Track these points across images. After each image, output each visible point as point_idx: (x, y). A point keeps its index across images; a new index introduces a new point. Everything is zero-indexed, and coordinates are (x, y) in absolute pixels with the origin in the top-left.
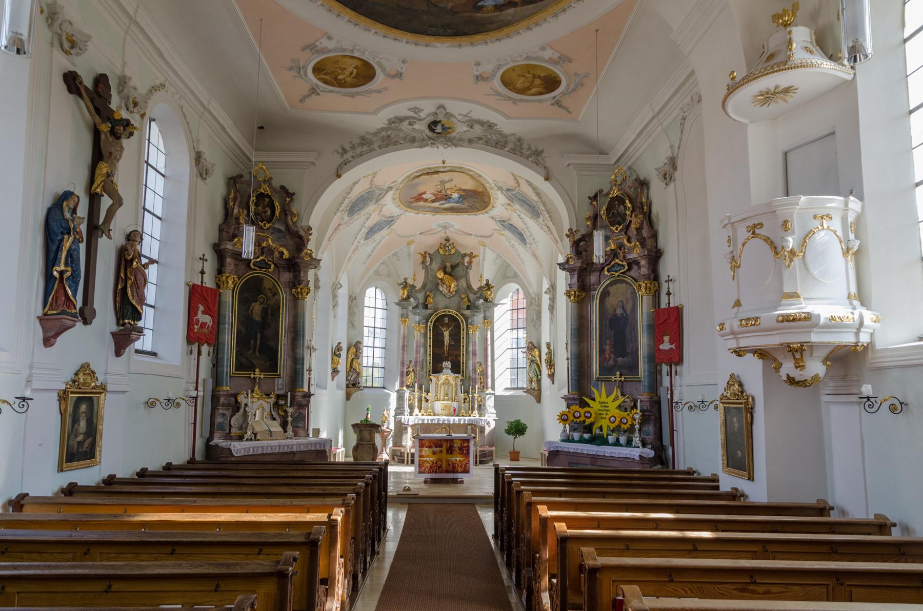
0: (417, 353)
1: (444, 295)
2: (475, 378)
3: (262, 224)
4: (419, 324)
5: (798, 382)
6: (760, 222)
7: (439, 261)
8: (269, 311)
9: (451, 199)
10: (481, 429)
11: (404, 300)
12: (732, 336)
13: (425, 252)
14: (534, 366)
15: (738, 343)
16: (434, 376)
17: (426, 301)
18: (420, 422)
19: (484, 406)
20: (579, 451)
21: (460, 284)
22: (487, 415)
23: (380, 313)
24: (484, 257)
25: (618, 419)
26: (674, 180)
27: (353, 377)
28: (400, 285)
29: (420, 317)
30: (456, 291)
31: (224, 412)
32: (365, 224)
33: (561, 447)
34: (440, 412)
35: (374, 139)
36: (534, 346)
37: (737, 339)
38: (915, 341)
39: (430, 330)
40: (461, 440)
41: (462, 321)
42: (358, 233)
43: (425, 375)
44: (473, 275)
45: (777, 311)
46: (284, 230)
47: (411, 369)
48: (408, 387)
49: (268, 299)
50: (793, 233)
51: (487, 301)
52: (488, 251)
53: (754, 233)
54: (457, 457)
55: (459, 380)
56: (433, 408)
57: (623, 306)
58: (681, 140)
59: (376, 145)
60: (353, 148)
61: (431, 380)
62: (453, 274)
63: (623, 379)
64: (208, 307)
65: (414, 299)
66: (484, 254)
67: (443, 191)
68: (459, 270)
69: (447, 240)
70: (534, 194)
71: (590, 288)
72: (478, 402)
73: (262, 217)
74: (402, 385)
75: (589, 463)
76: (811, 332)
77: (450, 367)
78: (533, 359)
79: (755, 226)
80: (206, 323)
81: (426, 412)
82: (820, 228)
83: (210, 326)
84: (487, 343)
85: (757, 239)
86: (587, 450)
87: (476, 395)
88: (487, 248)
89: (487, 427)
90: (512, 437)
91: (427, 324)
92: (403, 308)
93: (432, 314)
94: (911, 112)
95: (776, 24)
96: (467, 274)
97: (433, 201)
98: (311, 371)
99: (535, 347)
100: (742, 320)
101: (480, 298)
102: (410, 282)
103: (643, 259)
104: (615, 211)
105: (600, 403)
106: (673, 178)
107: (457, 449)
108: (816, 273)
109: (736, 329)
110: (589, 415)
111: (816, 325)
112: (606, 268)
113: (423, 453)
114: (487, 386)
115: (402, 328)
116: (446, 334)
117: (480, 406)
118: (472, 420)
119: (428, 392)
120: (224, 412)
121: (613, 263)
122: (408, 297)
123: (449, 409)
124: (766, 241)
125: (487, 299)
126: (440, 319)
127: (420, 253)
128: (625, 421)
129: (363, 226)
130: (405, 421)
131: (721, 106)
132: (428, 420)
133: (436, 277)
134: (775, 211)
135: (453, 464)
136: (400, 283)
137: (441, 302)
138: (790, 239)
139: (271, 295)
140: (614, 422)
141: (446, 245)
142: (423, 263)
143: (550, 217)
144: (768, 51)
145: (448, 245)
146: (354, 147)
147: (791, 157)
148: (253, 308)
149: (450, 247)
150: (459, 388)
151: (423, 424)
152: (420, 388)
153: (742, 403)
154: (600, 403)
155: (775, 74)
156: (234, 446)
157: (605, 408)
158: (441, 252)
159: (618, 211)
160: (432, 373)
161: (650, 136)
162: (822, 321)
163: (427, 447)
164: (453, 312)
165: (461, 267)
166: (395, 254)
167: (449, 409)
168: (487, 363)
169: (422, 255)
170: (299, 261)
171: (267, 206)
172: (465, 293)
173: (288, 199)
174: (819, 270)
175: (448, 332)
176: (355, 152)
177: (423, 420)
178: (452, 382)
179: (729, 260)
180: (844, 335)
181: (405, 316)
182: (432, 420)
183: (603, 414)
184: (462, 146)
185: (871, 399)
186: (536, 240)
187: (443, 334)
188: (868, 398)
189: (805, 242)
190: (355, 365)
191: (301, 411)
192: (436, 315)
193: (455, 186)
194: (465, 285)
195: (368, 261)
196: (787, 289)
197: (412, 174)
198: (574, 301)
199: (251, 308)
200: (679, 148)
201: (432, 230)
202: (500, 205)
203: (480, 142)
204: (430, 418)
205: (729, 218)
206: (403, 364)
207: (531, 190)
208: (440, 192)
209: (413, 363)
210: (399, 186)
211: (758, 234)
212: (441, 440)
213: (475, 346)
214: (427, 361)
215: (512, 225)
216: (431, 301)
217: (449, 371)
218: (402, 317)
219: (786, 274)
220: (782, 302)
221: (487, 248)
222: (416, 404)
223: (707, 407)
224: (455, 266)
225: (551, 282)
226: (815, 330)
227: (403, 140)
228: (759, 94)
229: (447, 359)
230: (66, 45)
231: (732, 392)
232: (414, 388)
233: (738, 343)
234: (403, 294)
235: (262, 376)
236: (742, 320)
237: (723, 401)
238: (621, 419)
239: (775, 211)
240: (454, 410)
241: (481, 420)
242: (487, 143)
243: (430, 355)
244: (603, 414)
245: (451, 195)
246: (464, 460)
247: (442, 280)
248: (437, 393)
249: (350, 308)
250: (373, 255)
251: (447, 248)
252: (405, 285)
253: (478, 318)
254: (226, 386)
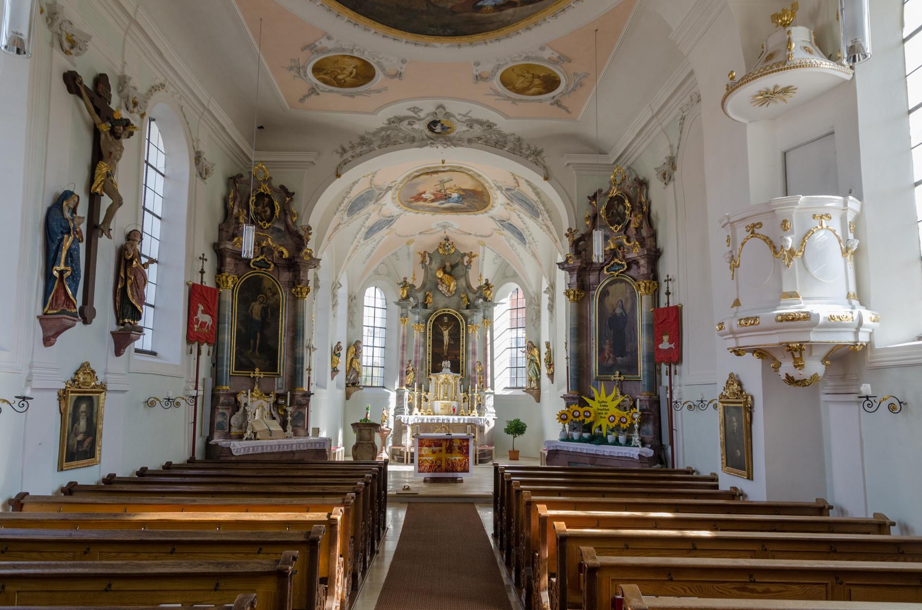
0: (416, 352)
1: (444, 294)
2: (475, 378)
3: (262, 224)
4: (419, 323)
5: (798, 381)
6: (759, 221)
7: (439, 261)
8: (269, 311)
9: (450, 199)
10: (480, 428)
11: (403, 299)
12: (731, 336)
13: (425, 252)
14: (534, 365)
15: (737, 343)
16: (434, 376)
17: (426, 301)
18: (420, 421)
19: (484, 405)
20: (578, 451)
21: (460, 284)
22: (486, 414)
23: (379, 313)
24: (483, 257)
25: (617, 419)
26: (674, 180)
27: (352, 377)
28: (400, 284)
29: (420, 316)
30: (455, 291)
31: (224, 411)
32: (364, 223)
33: (560, 446)
34: (440, 411)
35: (374, 139)
36: (533, 345)
37: (736, 338)
38: (914, 341)
39: (430, 329)
40: (460, 439)
41: (462, 321)
42: (358, 233)
43: (425, 374)
44: (472, 275)
45: (776, 310)
46: (283, 230)
47: (411, 369)
48: (407, 386)
49: (267, 299)
50: (792, 233)
51: (486, 301)
52: (488, 251)
53: (753, 233)
54: (456, 456)
55: (458, 379)
56: (432, 407)
57: (622, 306)
58: (680, 139)
59: (375, 145)
60: (353, 147)
61: (431, 379)
62: (453, 273)
63: (622, 378)
64: (208, 306)
65: (414, 299)
66: (484, 254)
67: (443, 191)
68: (459, 270)
69: (447, 239)
70: (534, 194)
71: (590, 288)
72: (478, 401)
73: (261, 217)
74: (401, 384)
75: (588, 462)
76: (810, 331)
77: (449, 366)
78: (533, 358)
79: (754, 226)
80: (206, 323)
81: (425, 411)
82: (819, 227)
83: (210, 325)
84: (486, 343)
85: (756, 238)
86: (587, 449)
87: (476, 395)
88: (486, 248)
89: (486, 426)
90: (511, 436)
91: (426, 324)
92: (402, 308)
93: (431, 314)
94: (910, 112)
95: (775, 24)
96: (466, 273)
97: (433, 201)
98: (310, 370)
99: (535, 347)
100: (742, 319)
101: (479, 298)
102: (410, 281)
103: (643, 258)
104: (615, 211)
105: (599, 402)
106: (672, 178)
107: (457, 448)
108: (815, 273)
109: (735, 328)
110: (589, 414)
111: (815, 325)
112: (605, 268)
113: (423, 453)
114: (486, 385)
115: (402, 328)
116: (446, 333)
117: (479, 405)
118: (472, 419)
119: (427, 391)
120: (224, 411)
121: (612, 263)
122: (408, 297)
123: (449, 408)
124: (765, 240)
125: (487, 299)
126: (439, 319)
127: (419, 253)
128: (625, 420)
129: (362, 226)
130: (404, 420)
131: (720, 106)
132: (427, 420)
133: (436, 277)
134: (774, 211)
135: (452, 463)
136: (399, 282)
137: (441, 302)
138: (789, 239)
139: (270, 294)
140: (614, 421)
141: (445, 244)
142: (423, 262)
143: (549, 216)
144: (767, 51)
145: (447, 244)
146: (354, 146)
147: (790, 157)
148: (253, 307)
149: (449, 246)
150: (459, 387)
151: (422, 423)
152: (420, 387)
153: (741, 403)
154: (599, 402)
155: (774, 74)
156: (234, 446)
157: (605, 408)
158: (441, 251)
159: (617, 211)
160: (432, 373)
161: (649, 136)
162: (821, 320)
163: (426, 446)
164: (453, 312)
165: (460, 266)
166: (395, 254)
167: (449, 408)
168: (486, 363)
169: (422, 254)
170: (299, 260)
171: (266, 206)
172: (465, 292)
173: (288, 199)
174: (818, 269)
175: (447, 331)
176: (355, 152)
177: (423, 420)
178: (452, 381)
179: (728, 260)
180: (843, 334)
181: (405, 315)
182: (432, 419)
183: (602, 414)
184: (462, 146)
185: (870, 399)
186: (535, 240)
187: (443, 334)
188: (867, 397)
189: (804, 241)
190: (355, 364)
191: (301, 410)
192: (436, 314)
193: (455, 186)
194: (464, 284)
195: (368, 261)
196: (786, 289)
197: (412, 174)
198: (573, 301)
199: (251, 307)
200: (678, 148)
201: (432, 229)
202: (499, 205)
203: (479, 142)
204: (430, 417)
205: (728, 217)
206: (402, 363)
207: (531, 189)
208: (440, 191)
209: (413, 363)
210: (398, 186)
211: (757, 234)
212: (440, 440)
213: (475, 346)
214: (426, 360)
215: (511, 225)
216: (431, 300)
217: (449, 370)
218: (401, 317)
219: (785, 273)
220: (781, 302)
221: (486, 248)
222: (416, 403)
223: (706, 406)
224: (454, 265)
225: (550, 281)
226: (814, 329)
227: (403, 140)
228: (758, 93)
229: (446, 359)
230: (66, 45)
231: (731, 391)
232: (414, 387)
233: (737, 343)
234: (403, 294)
235: (262, 376)
236: (742, 319)
237: (722, 400)
238: (621, 419)
239: (774, 211)
240: (454, 410)
241: (481, 419)
242: (486, 142)
243: (429, 354)
244: (602, 414)
245: (451, 194)
246: (464, 459)
247: (441, 279)
248: (436, 392)
249: (349, 307)
250: (373, 254)
251: (446, 248)
252: (405, 284)
253: (478, 318)
254: (226, 385)
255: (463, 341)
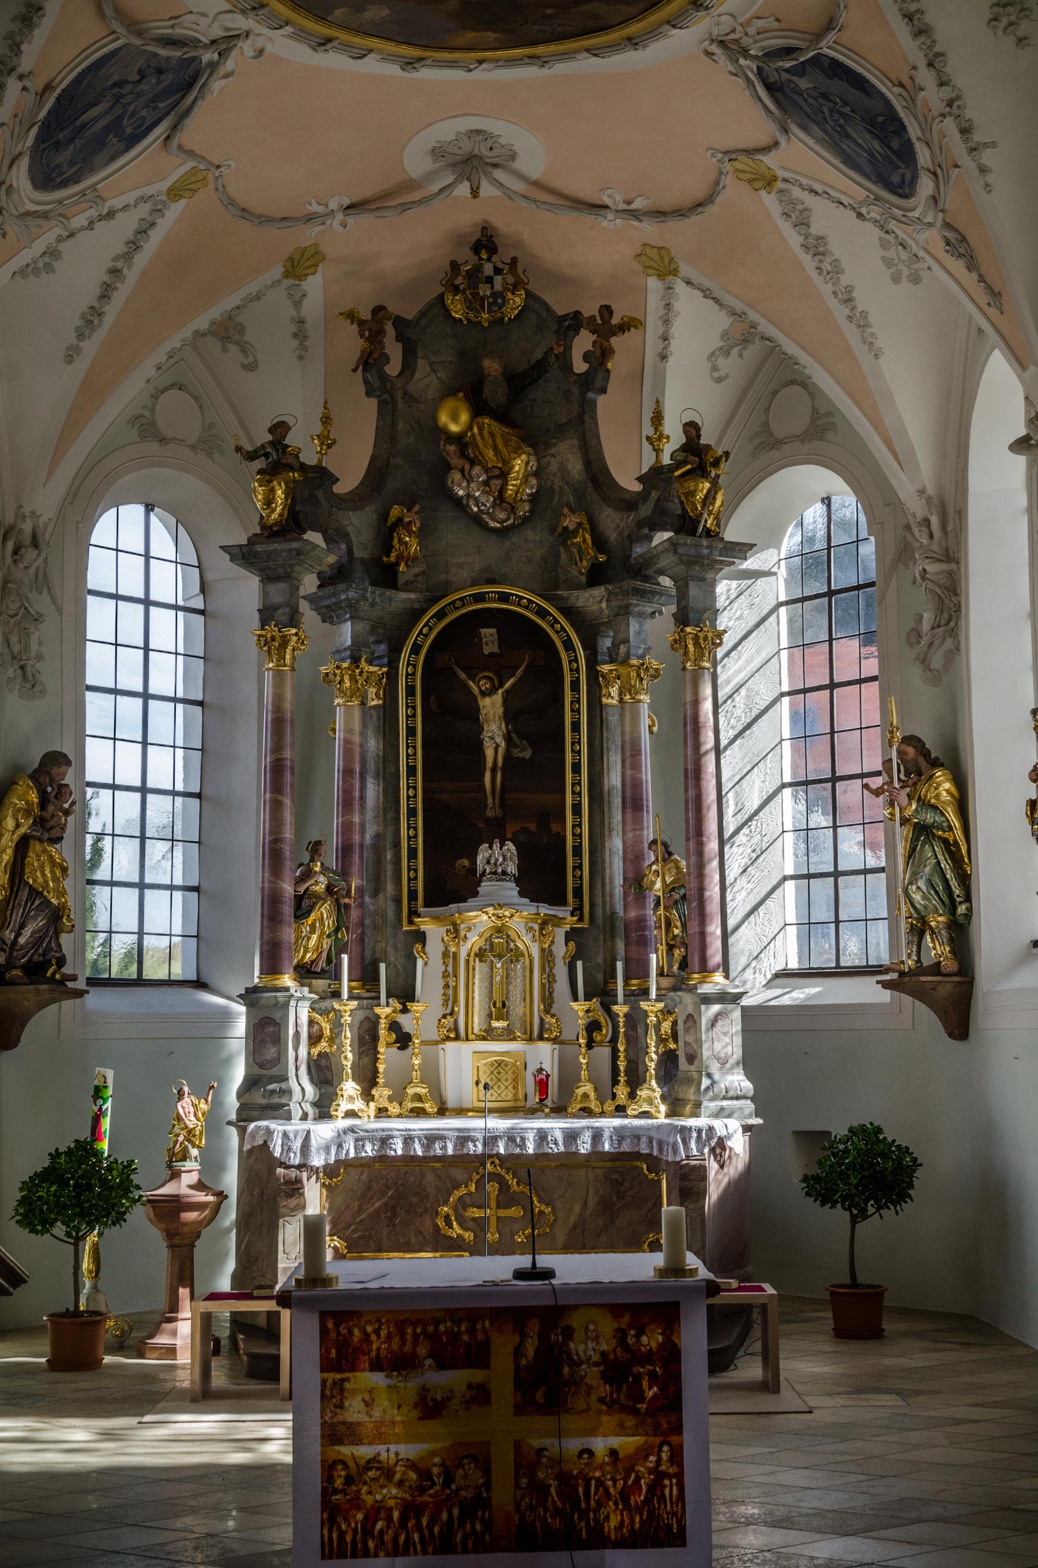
0: (347, 804)
2: (641, 923)
4: (355, 661)
10: (684, 1177)
11: (271, 532)
13: (378, 310)
14: (933, 854)
16: (437, 918)
17: (388, 550)
18: (369, 1150)
19: (692, 1058)
22: (709, 1105)
24: (665, 338)
27: (27, 932)
28: (252, 456)
29: (363, 626)
30: (534, 499)
34: (471, 1095)
36: (925, 753)
39: (410, 691)
40: (616, 1310)
41: (569, 645)
43: (391, 914)
47: (320, 885)
48: (305, 973)
52: (686, 299)
54: (593, 1432)
55: (560, 934)
56: (433, 1078)
61: (421, 937)
66: (667, 322)
72: (661, 1040)
74: (272, 965)
77: (512, 868)
78: (929, 817)
81: (398, 1098)
84: (697, 745)
87: (652, 1007)
88: (680, 287)
89: (713, 1166)
90: (839, 1216)
92: (268, 578)
93: (416, 615)
99: (935, 764)
101: (655, 526)
107: (593, 1375)
113: (354, 1411)
114: (704, 960)
115: (268, 677)
116: (492, 706)
117: (669, 1060)
118: (636, 1135)
119: (405, 994)
123: (516, 1081)
125: (695, 522)
130: (287, 1149)
132: (408, 1140)
135: (566, 1480)
141: (478, 269)
149: (498, 280)
150: (561, 972)
151: (382, 1159)
152: (367, 976)
158: (457, 309)
160: (426, 905)
163: (376, 1366)
167: (516, 1081)
168: (700, 845)
169: (361, 323)
175: (498, 697)
177: (385, 1141)
178: (528, 943)
181: (281, 615)
182: (431, 1139)
186: (978, 137)
187: (478, 710)
190: (38, 873)
192: (440, 615)
194: (575, 467)
195: (90, 348)
204: (420, 1125)
206: (274, 857)
209: (331, 857)
212: (473, 1315)
213: (636, 766)
214: (397, 844)
215: (836, 69)
217: (510, 890)
218: (264, 623)
221: (680, 287)
222: (348, 1060)
229: (496, 832)
232: (338, 977)
234: (269, 502)
240: (542, 1086)
241: (685, 1131)
243: (412, 813)
246: (643, 1452)
247: (458, 440)
248: (450, 999)
250: (112, 310)
251: (484, 290)
255: (577, 783)
